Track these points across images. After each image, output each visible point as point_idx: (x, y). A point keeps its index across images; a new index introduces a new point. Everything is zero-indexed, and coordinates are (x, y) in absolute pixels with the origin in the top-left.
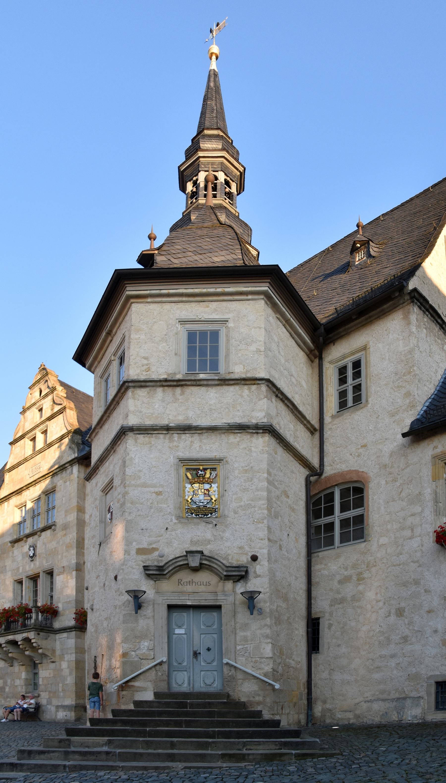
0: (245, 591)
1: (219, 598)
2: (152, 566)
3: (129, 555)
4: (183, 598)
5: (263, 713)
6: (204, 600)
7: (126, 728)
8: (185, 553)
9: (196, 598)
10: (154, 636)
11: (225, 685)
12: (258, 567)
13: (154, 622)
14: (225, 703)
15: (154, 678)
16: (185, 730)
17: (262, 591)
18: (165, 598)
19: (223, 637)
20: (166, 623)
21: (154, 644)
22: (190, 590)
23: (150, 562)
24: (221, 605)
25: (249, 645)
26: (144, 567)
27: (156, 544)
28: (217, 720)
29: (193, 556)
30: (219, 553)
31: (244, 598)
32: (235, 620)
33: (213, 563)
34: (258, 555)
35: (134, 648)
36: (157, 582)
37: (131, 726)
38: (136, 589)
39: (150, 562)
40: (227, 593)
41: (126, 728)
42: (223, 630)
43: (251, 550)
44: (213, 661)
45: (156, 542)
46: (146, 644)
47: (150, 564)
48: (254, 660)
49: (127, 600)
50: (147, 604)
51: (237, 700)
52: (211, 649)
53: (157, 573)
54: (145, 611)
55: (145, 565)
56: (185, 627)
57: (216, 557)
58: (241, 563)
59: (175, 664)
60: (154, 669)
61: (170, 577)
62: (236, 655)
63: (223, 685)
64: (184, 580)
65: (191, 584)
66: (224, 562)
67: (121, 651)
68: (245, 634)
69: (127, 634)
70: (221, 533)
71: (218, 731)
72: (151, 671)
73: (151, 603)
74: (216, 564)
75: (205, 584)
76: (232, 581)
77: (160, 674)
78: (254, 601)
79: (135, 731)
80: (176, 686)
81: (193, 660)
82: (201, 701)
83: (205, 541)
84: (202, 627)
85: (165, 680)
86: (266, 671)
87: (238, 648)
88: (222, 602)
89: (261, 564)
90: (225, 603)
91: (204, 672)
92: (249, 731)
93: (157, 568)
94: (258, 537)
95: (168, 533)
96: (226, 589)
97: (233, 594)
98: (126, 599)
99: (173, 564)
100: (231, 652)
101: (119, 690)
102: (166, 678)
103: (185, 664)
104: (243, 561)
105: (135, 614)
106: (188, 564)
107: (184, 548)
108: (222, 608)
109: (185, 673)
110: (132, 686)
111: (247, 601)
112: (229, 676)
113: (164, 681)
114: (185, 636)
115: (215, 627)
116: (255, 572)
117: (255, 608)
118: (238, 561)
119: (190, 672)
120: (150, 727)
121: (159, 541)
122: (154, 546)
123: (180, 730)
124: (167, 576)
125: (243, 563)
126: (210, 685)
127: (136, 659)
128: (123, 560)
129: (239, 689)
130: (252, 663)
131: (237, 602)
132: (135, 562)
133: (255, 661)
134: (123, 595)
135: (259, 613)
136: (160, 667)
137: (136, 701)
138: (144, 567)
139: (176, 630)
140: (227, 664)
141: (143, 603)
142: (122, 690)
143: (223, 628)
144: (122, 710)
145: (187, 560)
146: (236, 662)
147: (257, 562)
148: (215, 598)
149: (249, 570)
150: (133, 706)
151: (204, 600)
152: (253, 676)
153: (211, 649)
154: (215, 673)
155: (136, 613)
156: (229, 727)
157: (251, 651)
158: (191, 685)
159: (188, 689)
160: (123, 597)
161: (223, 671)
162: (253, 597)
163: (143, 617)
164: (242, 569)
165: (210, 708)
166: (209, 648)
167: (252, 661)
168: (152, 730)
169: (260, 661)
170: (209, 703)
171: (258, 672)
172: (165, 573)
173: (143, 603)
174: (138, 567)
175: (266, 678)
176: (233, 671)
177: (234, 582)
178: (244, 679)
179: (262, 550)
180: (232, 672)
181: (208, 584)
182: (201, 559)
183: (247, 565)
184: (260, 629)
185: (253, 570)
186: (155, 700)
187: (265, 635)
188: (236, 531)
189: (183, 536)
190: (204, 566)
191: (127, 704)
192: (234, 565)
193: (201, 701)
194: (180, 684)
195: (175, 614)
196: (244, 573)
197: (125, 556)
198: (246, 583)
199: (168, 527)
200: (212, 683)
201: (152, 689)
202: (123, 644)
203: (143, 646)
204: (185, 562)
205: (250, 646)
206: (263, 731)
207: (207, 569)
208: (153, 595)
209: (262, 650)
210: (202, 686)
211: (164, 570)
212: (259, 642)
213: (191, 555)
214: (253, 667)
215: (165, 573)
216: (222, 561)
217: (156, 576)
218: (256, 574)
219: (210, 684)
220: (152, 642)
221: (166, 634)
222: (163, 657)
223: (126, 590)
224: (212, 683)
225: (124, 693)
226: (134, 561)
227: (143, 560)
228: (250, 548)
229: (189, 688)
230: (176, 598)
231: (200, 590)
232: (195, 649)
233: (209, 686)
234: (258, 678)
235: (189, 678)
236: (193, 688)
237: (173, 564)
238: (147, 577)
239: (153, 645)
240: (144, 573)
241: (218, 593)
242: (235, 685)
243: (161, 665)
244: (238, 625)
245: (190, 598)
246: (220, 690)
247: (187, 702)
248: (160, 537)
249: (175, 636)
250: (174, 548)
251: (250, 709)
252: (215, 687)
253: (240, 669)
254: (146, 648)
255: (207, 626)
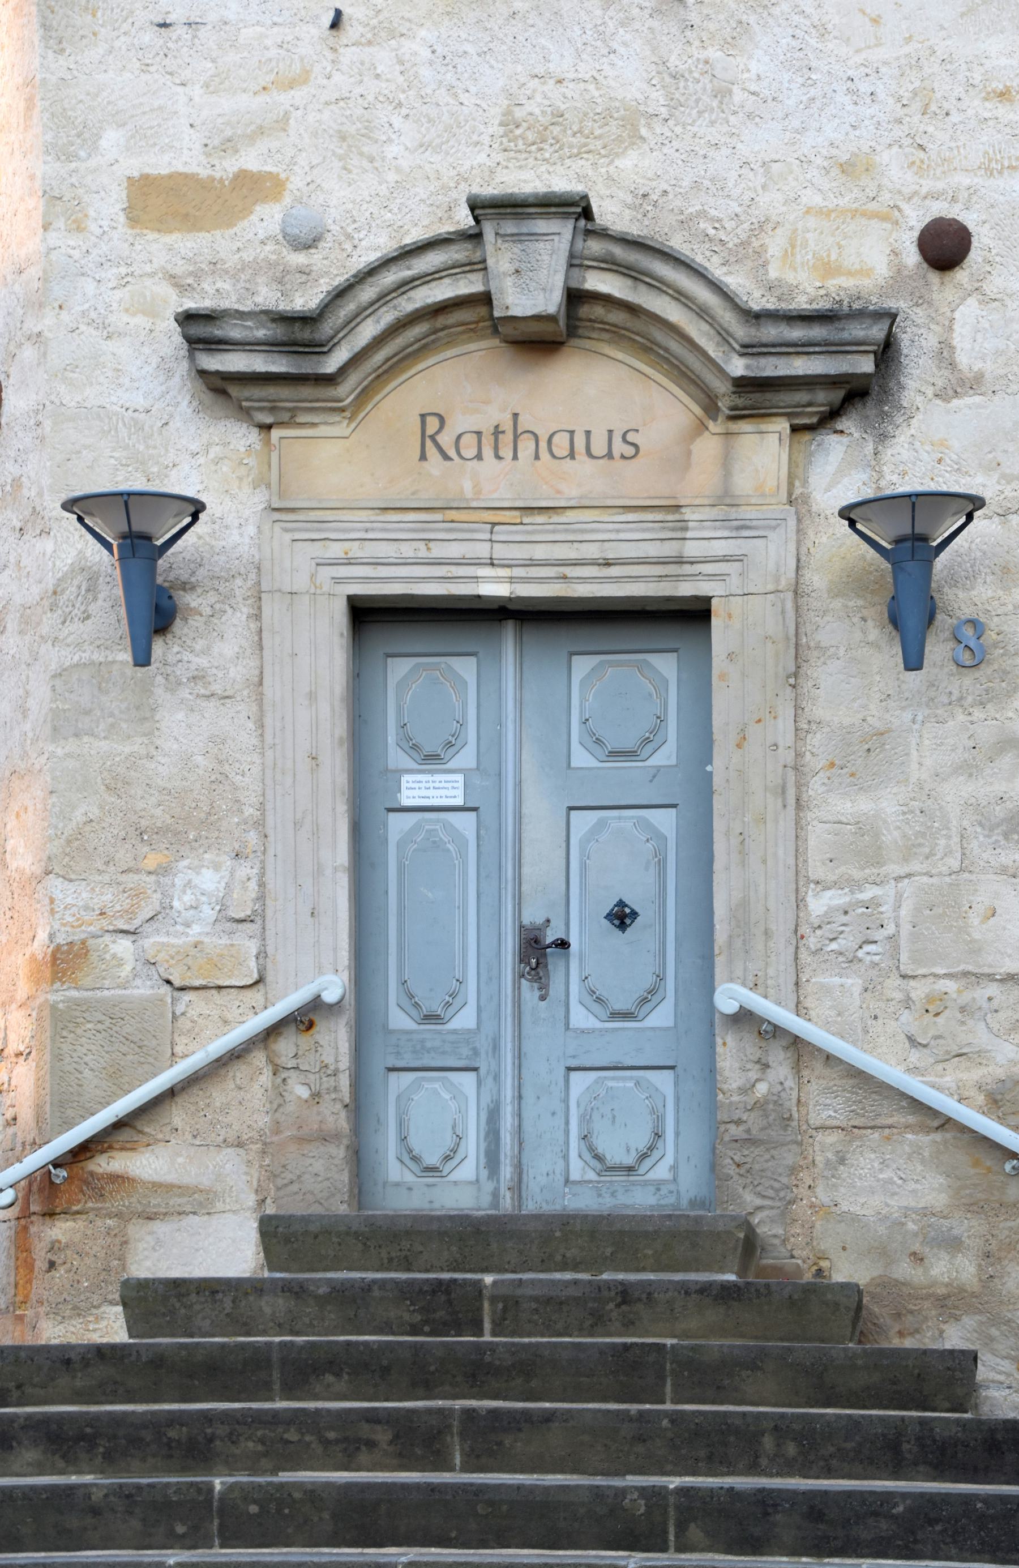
0: (869, 493)
1: (692, 549)
2: (241, 315)
3: (79, 227)
4: (454, 550)
5: (982, 1373)
6: (594, 562)
7: (74, 1479)
8: (464, 219)
9: (540, 552)
10: (260, 824)
11: (732, 1170)
12: (968, 312)
13: (261, 725)
14: (726, 1293)
15: (263, 1121)
16: (465, 1488)
17: (987, 494)
18: (336, 550)
19: (719, 826)
20: (341, 728)
21: (262, 885)
22: (502, 494)
23: (225, 285)
24: (708, 600)
25: (887, 892)
26: (187, 319)
27: (262, 145)
28: (676, 1418)
29: (517, 238)
30: (702, 214)
31: (865, 546)
32: (798, 708)
33: (659, 286)
34: (970, 220)
35: (130, 913)
36: (276, 433)
37: (110, 1461)
38: (138, 485)
39: (225, 285)
40: (748, 513)
41: (74, 1479)
42: (717, 781)
43: (927, 185)
44: (649, 998)
45: (261, 131)
46: (209, 880)
47: (225, 304)
48: (919, 990)
49: (80, 568)
50: (212, 598)
51: (808, 1277)
52: (634, 914)
53: (278, 365)
54: (200, 645)
55: (190, 304)
56: (466, 757)
57: (677, 243)
58: (848, 283)
59: (400, 1020)
60: (259, 1058)
61: (365, 395)
62: (803, 955)
63: (713, 1167)
64: (460, 422)
65: (507, 452)
66: (735, 281)
67: (42, 936)
68: (864, 805)
69: (78, 816)
70: (713, 53)
71: (684, 1491)
72: (240, 1072)
73: (240, 587)
74: (680, 296)
75: (599, 447)
76: (783, 425)
77: (304, 1093)
78: (929, 563)
79: (129, 1496)
80: (409, 1178)
81: (517, 988)
82: (568, 1276)
83: (606, 117)
84: (581, 758)
85: (337, 1136)
86: (1000, 1073)
87: (818, 904)
88: (712, 577)
89: (991, 288)
90: (734, 584)
91: (593, 1075)
92: (888, 1496)
93: (278, 332)
94: (977, 77)
95: (348, 55)
96: (743, 483)
97: (792, 523)
98: (68, 558)
99: (383, 298)
100: (767, 933)
101: (25, 1215)
102: (342, 1122)
103: (465, 1019)
104: (866, 272)
105: (130, 670)
106: (485, 299)
107: (461, 178)
108: (715, 621)
109: (467, 1081)
110: (116, 1179)
111: (886, 565)
112: (760, 1106)
113: (325, 1138)
114: (466, 823)
115: (665, 756)
116: (945, 354)
117: (940, 617)
118: (829, 269)
119: (497, 1078)
120: (232, 1470)
121: (283, 123)
122: (251, 160)
123: (432, 1488)
124: (346, 390)
125: (866, 284)
126: (630, 1169)
127: (144, 989)
128: (34, 272)
129: (822, 1195)
130: (906, 1016)
131: (816, 580)
132: (123, 283)
133: (930, 999)
134: (45, 532)
135: (966, 658)
136: (305, 1041)
137: (144, 1285)
138: (187, 319)
139: (406, 779)
140: (744, 1018)
141: (186, 586)
142: (50, 1214)
143: (718, 767)
144: (47, 1349)
145: (480, 266)
146: (799, 1009)
147: (961, 275)
148: (668, 549)
149: (904, 340)
150: (121, 1322)
151: (594, 562)
152: (917, 1105)
153: (634, 914)
154: (663, 1081)
155: (142, 659)
156: (753, 1468)
157: (906, 929)
158: (506, 1171)
159: (486, 1200)
160: (47, 545)
161: (712, 1070)
162: (924, 539)
163: (184, 693)
164: (857, 331)
165: (629, 1325)
166: (621, 904)
167: (907, 1003)
168: (247, 1493)
169: (966, 997)
170: (625, 1294)
171: (948, 1080)
172: (331, 364)
173: (186, 586)
174: (141, 321)
175: (1001, 1120)
176: (781, 1070)
177: (795, 429)
178: (849, 1130)
179: (1000, 182)
180: (772, 1075)
181: (619, 447)
182: (575, 262)
183: (891, 304)
184: (968, 769)
185: (930, 341)
186: (266, 1274)
187: (999, 812)
188: (823, 31)
189: (450, 77)
190: (598, 311)
191: (78, 1312)
192: (801, 303)
193: (568, 1276)
194: (432, 1159)
195: (399, 669)
196: (866, 365)
197: (53, 238)
198: (883, 438)
199: (347, 11)
200: (643, 1157)
201: (251, 1200)
202: (56, 885)
203: (188, 898)
204: (468, 286)
205: (899, 898)
206: (988, 1500)
207: (617, 335)
208: (251, 530)
209: (975, 920)
210: (575, 1176)
211: (319, 348)
212: (955, 865)
213: (509, 227)
214: (911, 1040)
215: (331, 364)
216: (718, 272)
217: (271, 391)
218: (952, 365)
219: (629, 1160)
220: (246, 870)
221: (342, 808)
222: (320, 971)
223: (64, 496)
224: (643, 1157)
225: (60, 1230)
226: (111, 273)
227: (180, 268)
228: (920, 169)
229: (488, 1187)
230: (407, 550)
231: (570, 493)
232: (532, 916)
233: (620, 1178)
234: (946, 1123)
235: (493, 1116)
236: (518, 1186)
237: (383, 298)
238: (208, 397)
239: (253, 885)
240: (185, 364)
241: (688, 514)
242: (793, 1170)
243: (311, 1025)
244: (816, 740)
245: (501, 552)
246: (693, 1203)
247: (478, 1284)
248: (291, 84)
249: (398, 825)
250: (392, 177)
251: (896, 1343)
252: (658, 1185)
253: (829, 1059)
254: (209, 913)
255: (615, 754)
